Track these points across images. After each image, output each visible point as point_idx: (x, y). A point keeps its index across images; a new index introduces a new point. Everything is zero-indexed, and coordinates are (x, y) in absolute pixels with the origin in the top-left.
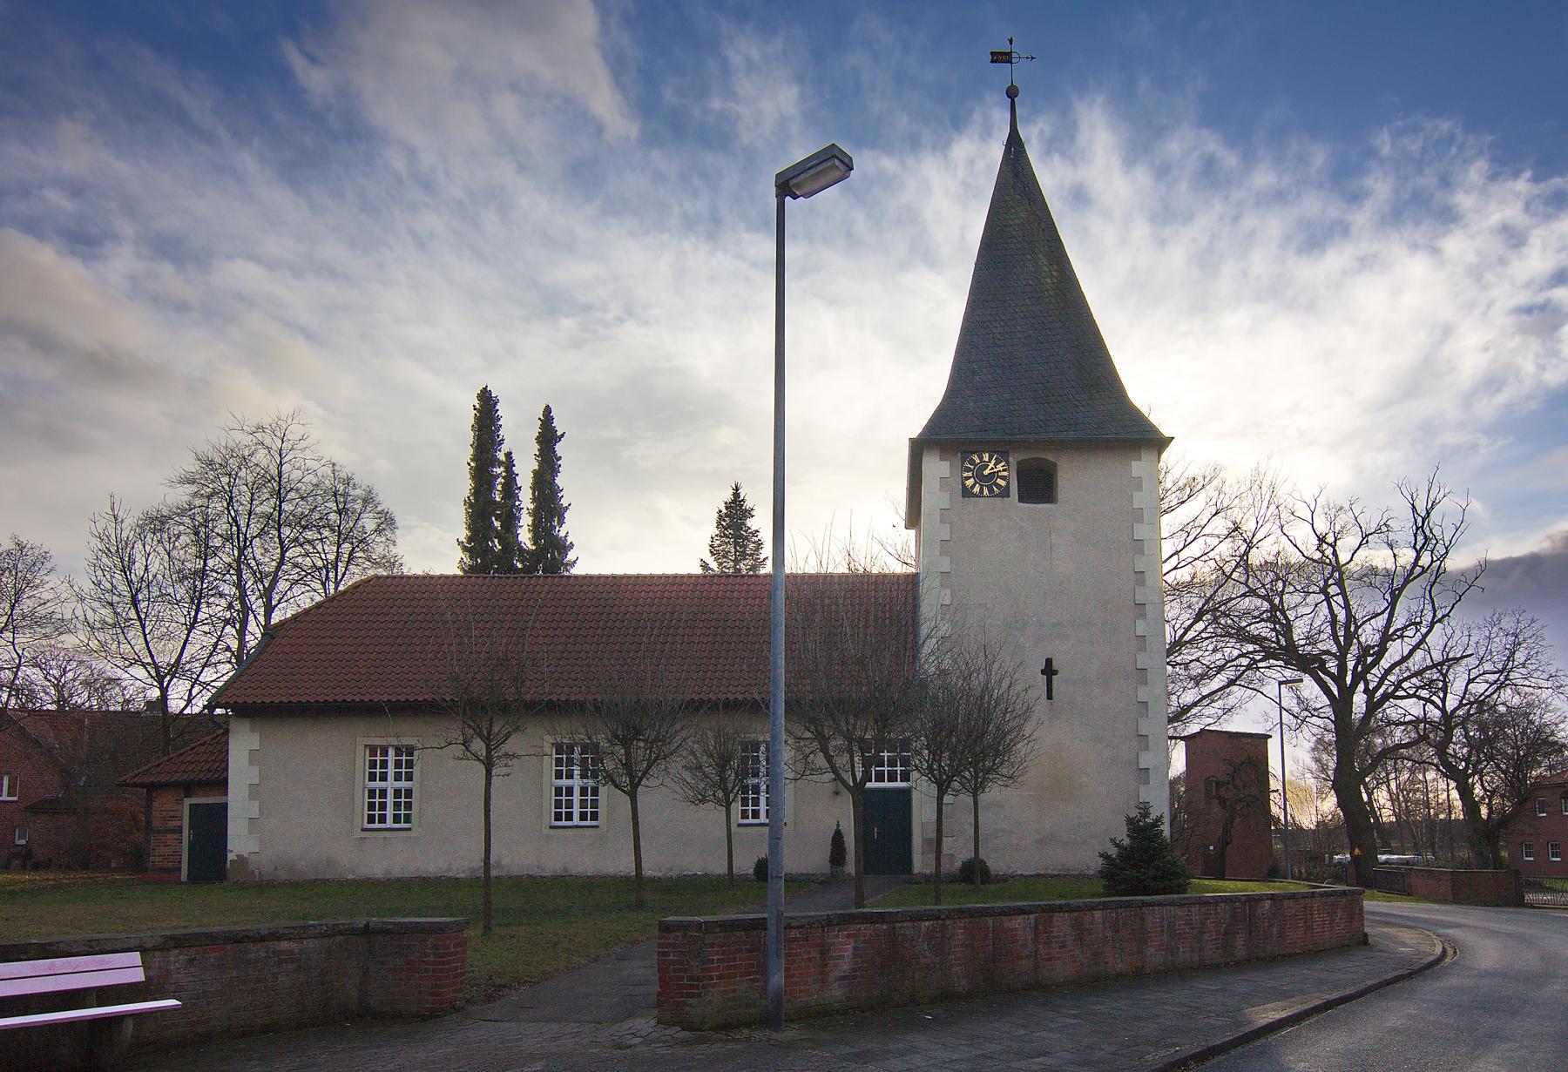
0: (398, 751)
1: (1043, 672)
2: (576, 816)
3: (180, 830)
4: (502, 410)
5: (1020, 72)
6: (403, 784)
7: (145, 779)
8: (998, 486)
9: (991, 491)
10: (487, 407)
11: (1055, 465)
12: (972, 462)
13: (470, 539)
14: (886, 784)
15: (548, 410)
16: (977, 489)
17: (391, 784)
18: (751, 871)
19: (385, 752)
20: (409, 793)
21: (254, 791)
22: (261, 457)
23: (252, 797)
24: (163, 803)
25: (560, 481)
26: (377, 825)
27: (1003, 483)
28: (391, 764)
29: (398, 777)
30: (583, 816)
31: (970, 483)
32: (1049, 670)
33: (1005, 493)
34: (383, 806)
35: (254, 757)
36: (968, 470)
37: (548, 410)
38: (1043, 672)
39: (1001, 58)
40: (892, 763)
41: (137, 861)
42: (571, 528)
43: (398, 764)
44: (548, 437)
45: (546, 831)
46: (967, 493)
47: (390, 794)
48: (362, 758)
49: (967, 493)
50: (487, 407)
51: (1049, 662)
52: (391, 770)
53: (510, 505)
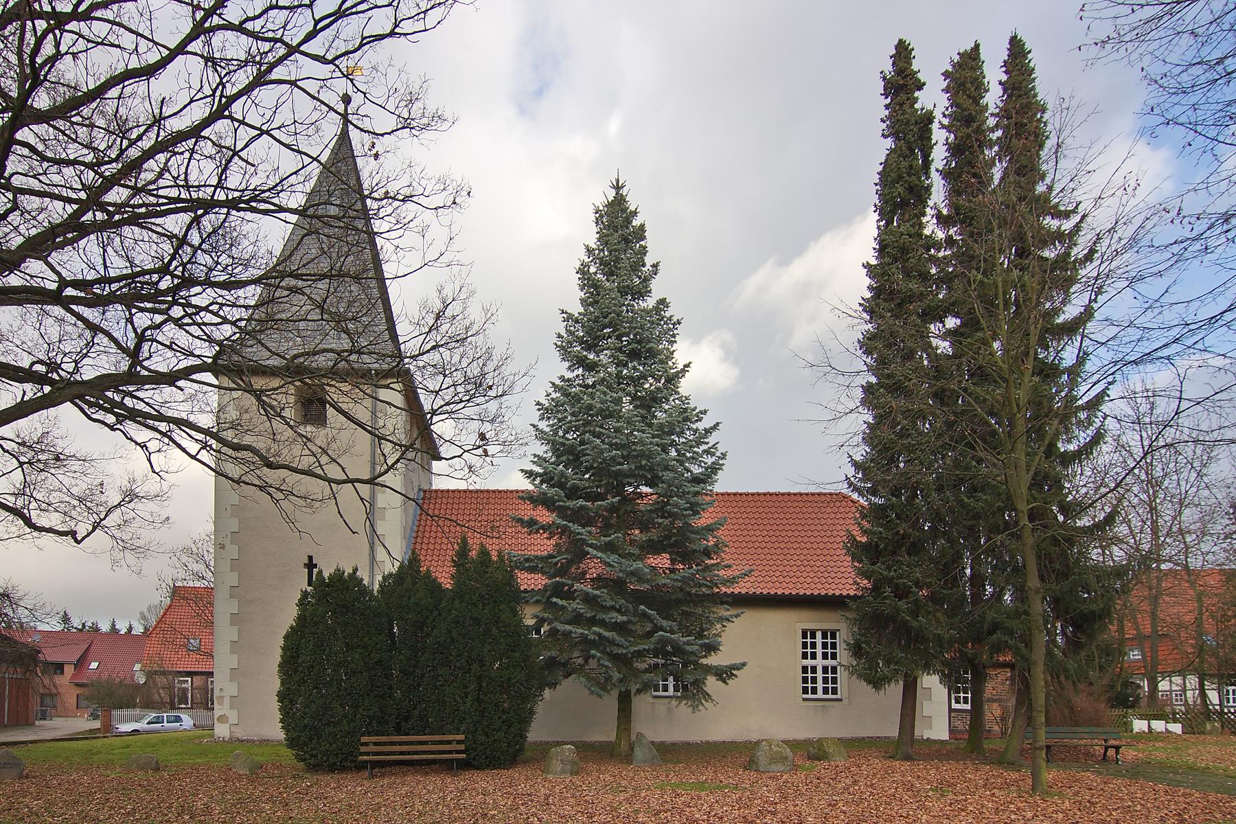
17: (819, 662)
28: (819, 646)
43: (825, 646)
51: (310, 558)
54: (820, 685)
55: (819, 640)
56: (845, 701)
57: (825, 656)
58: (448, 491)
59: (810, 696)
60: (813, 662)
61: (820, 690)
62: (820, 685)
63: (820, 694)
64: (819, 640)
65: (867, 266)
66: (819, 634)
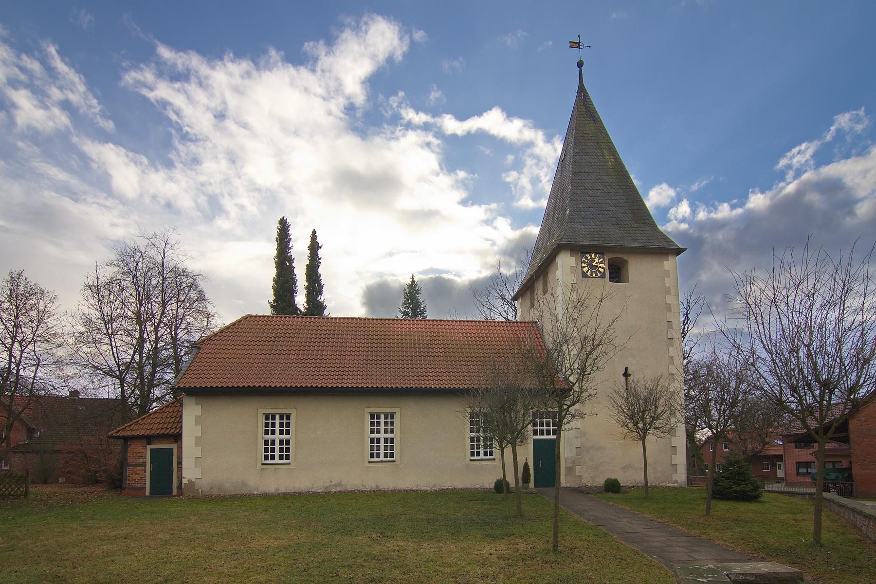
0: (282, 418)
1: (624, 375)
2: (382, 455)
3: (144, 464)
4: (291, 231)
5: (585, 54)
6: (389, 435)
7: (120, 434)
8: (600, 272)
9: (596, 274)
10: (284, 229)
11: (626, 262)
12: (586, 258)
13: (274, 301)
14: (545, 437)
15: (314, 232)
16: (589, 273)
17: (277, 437)
18: (493, 486)
19: (274, 418)
20: (288, 442)
21: (198, 441)
22: (152, 253)
23: (197, 444)
24: (134, 449)
25: (320, 270)
26: (375, 459)
27: (602, 270)
28: (277, 425)
29: (386, 431)
30: (386, 456)
31: (585, 269)
32: (626, 374)
33: (603, 276)
34: (273, 450)
35: (198, 420)
36: (584, 262)
37: (314, 232)
38: (624, 375)
39: (576, 45)
40: (548, 425)
41: (116, 483)
42: (325, 297)
43: (281, 425)
44: (314, 247)
45: (367, 464)
46: (584, 275)
47: (277, 442)
48: (262, 421)
49: (584, 275)
50: (284, 229)
51: (626, 369)
52: (382, 427)
53: (294, 282)
54: (277, 454)
55: (278, 421)
56: (397, 463)
57: (386, 431)
58: (352, 319)
59: (476, 457)
60: (273, 437)
61: (277, 457)
62: (277, 454)
63: (277, 460)
64: (278, 421)
65: (464, 203)
66: (277, 417)
